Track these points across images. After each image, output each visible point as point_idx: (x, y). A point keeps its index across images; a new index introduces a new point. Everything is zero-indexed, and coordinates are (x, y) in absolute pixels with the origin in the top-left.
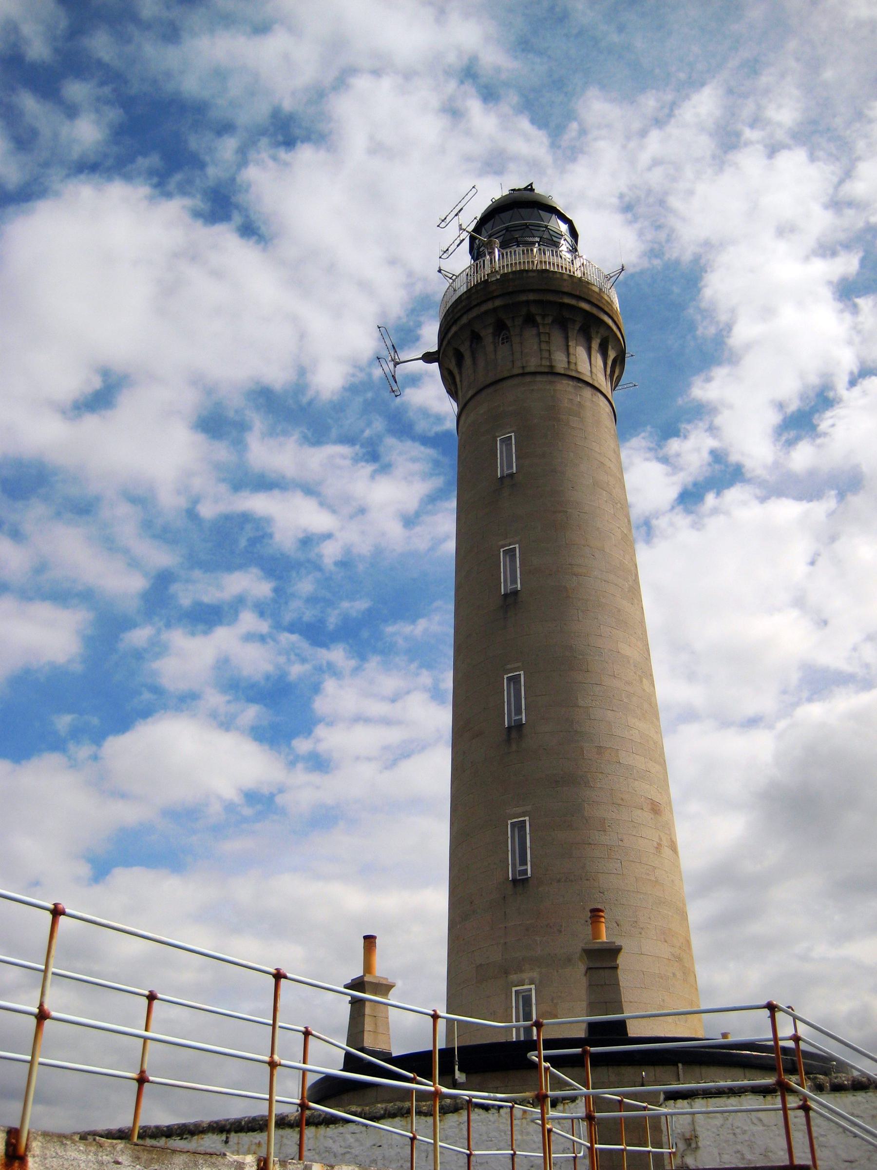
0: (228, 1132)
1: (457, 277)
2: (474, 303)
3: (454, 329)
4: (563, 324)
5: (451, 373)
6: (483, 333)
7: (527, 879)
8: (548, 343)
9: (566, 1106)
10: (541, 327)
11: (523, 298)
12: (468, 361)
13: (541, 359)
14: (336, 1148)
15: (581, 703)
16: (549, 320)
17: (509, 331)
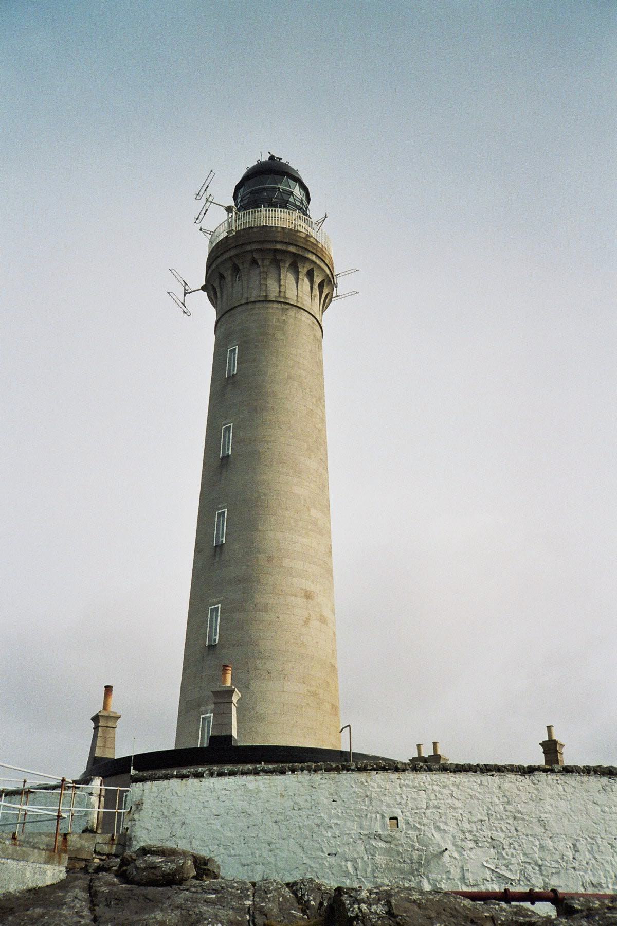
3: (219, 260)
6: (225, 275)
8: (266, 279)
11: (249, 248)
15: (261, 528)
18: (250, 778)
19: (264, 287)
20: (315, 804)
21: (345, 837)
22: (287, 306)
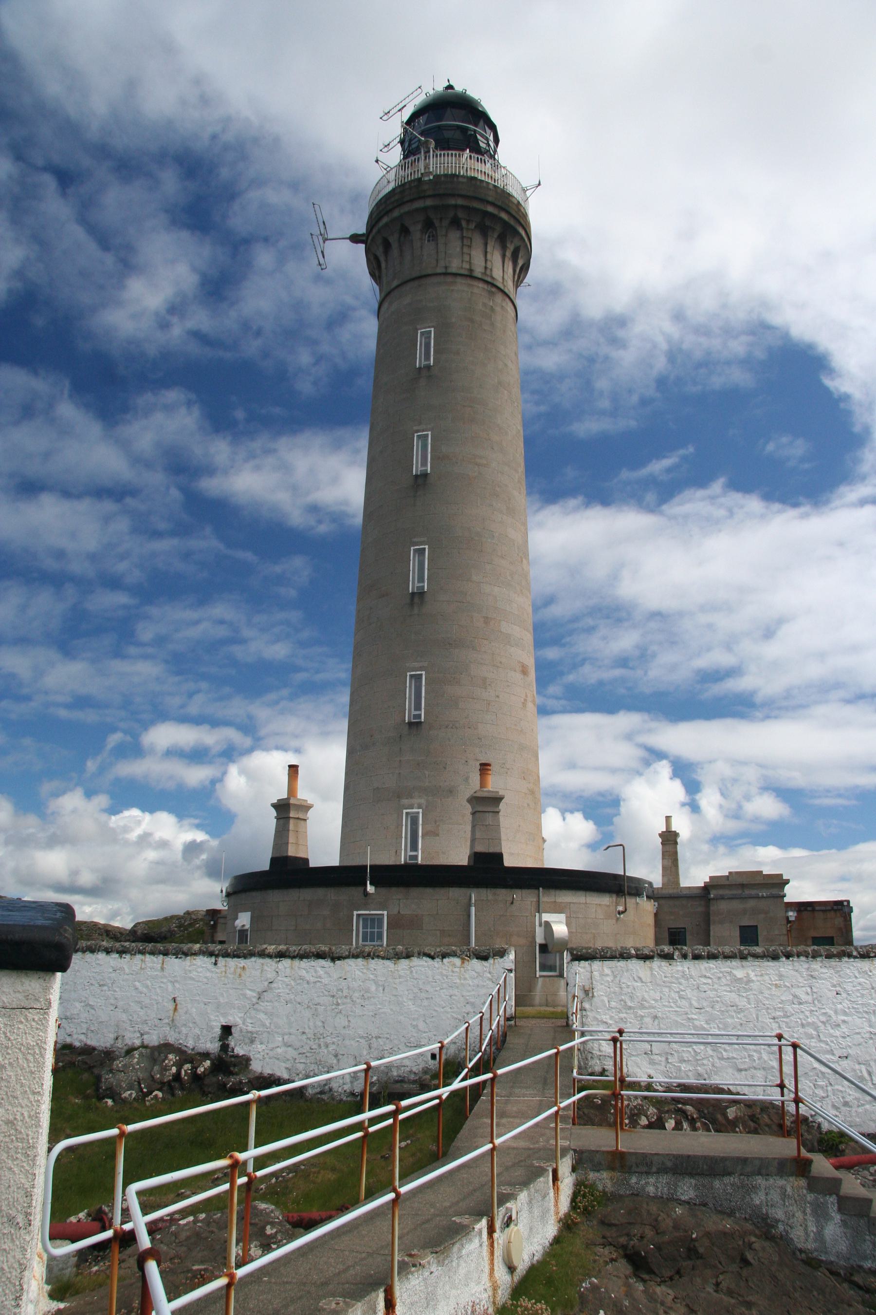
0: (217, 956)
1: (392, 169)
3: (385, 220)
4: (484, 231)
5: (377, 258)
6: (412, 229)
7: (421, 722)
8: (470, 247)
12: (395, 252)
13: (462, 261)
14: (308, 977)
16: (472, 226)
17: (436, 231)
18: (735, 963)
19: (466, 258)
20: (817, 999)
21: (856, 1036)
22: (494, 289)
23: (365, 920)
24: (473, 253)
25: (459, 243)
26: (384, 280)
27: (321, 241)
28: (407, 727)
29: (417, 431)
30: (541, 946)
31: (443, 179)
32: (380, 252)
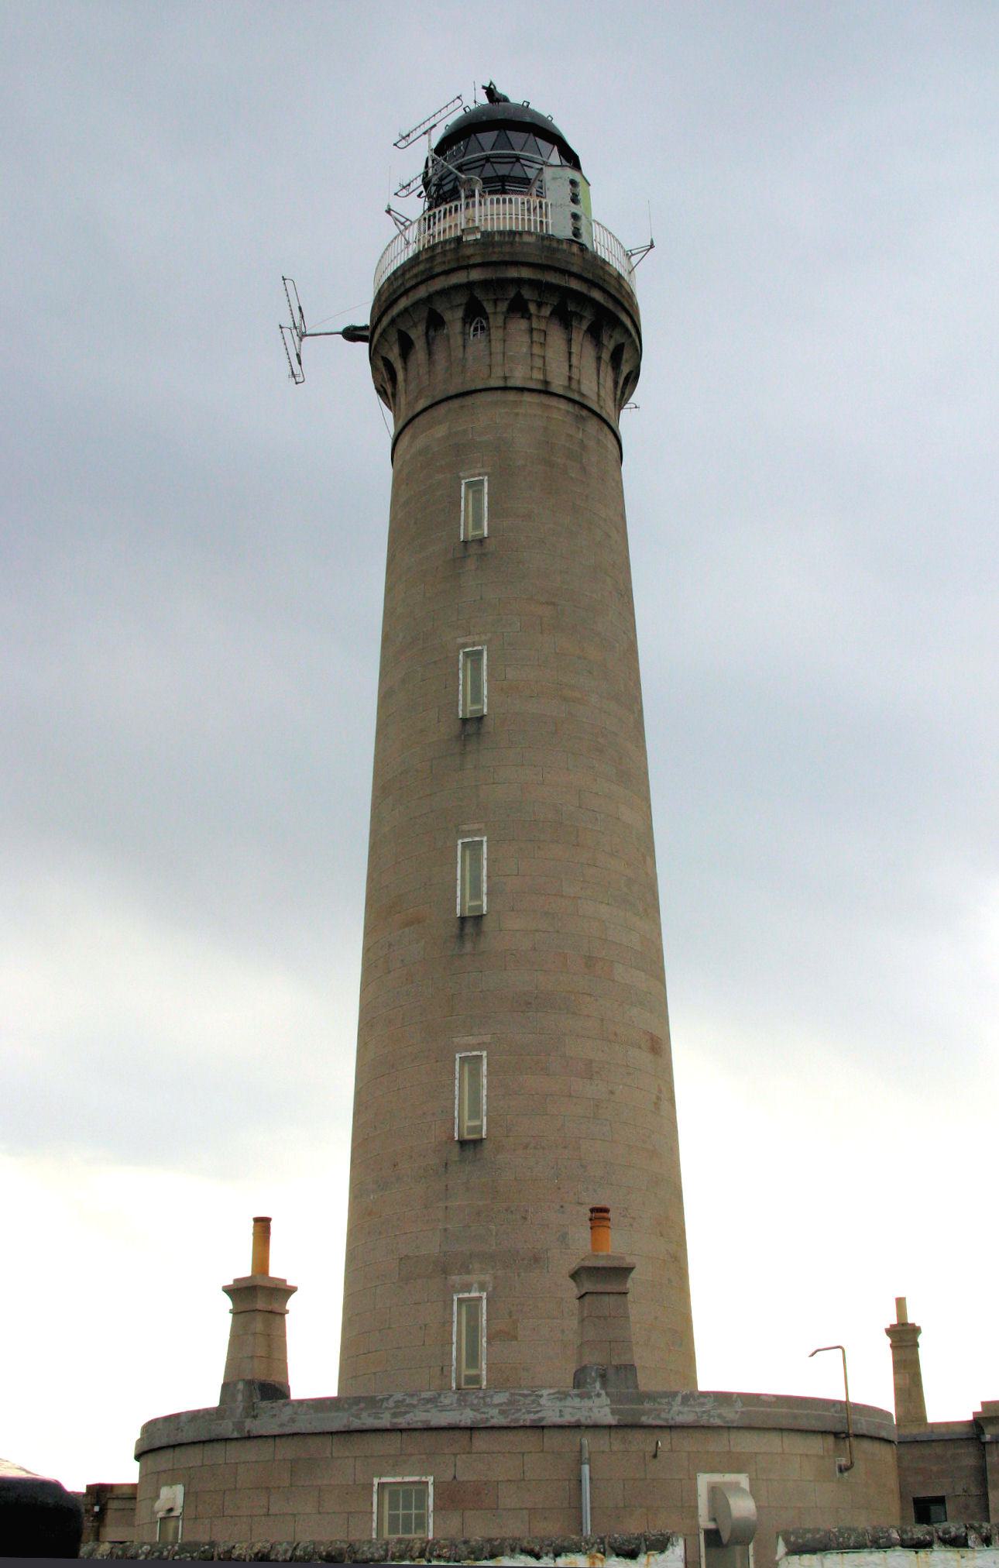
2: (438, 270)
3: (403, 303)
4: (564, 318)
6: (448, 316)
7: (481, 1140)
8: (543, 345)
9: (652, 1559)
10: (534, 320)
12: (419, 354)
16: (546, 311)
17: (487, 319)
22: (584, 413)
23: (394, 1496)
24: (550, 354)
25: (526, 339)
26: (402, 400)
27: (297, 339)
28: (457, 1148)
29: (465, 645)
30: (708, 1532)
31: (497, 238)
32: (394, 355)
